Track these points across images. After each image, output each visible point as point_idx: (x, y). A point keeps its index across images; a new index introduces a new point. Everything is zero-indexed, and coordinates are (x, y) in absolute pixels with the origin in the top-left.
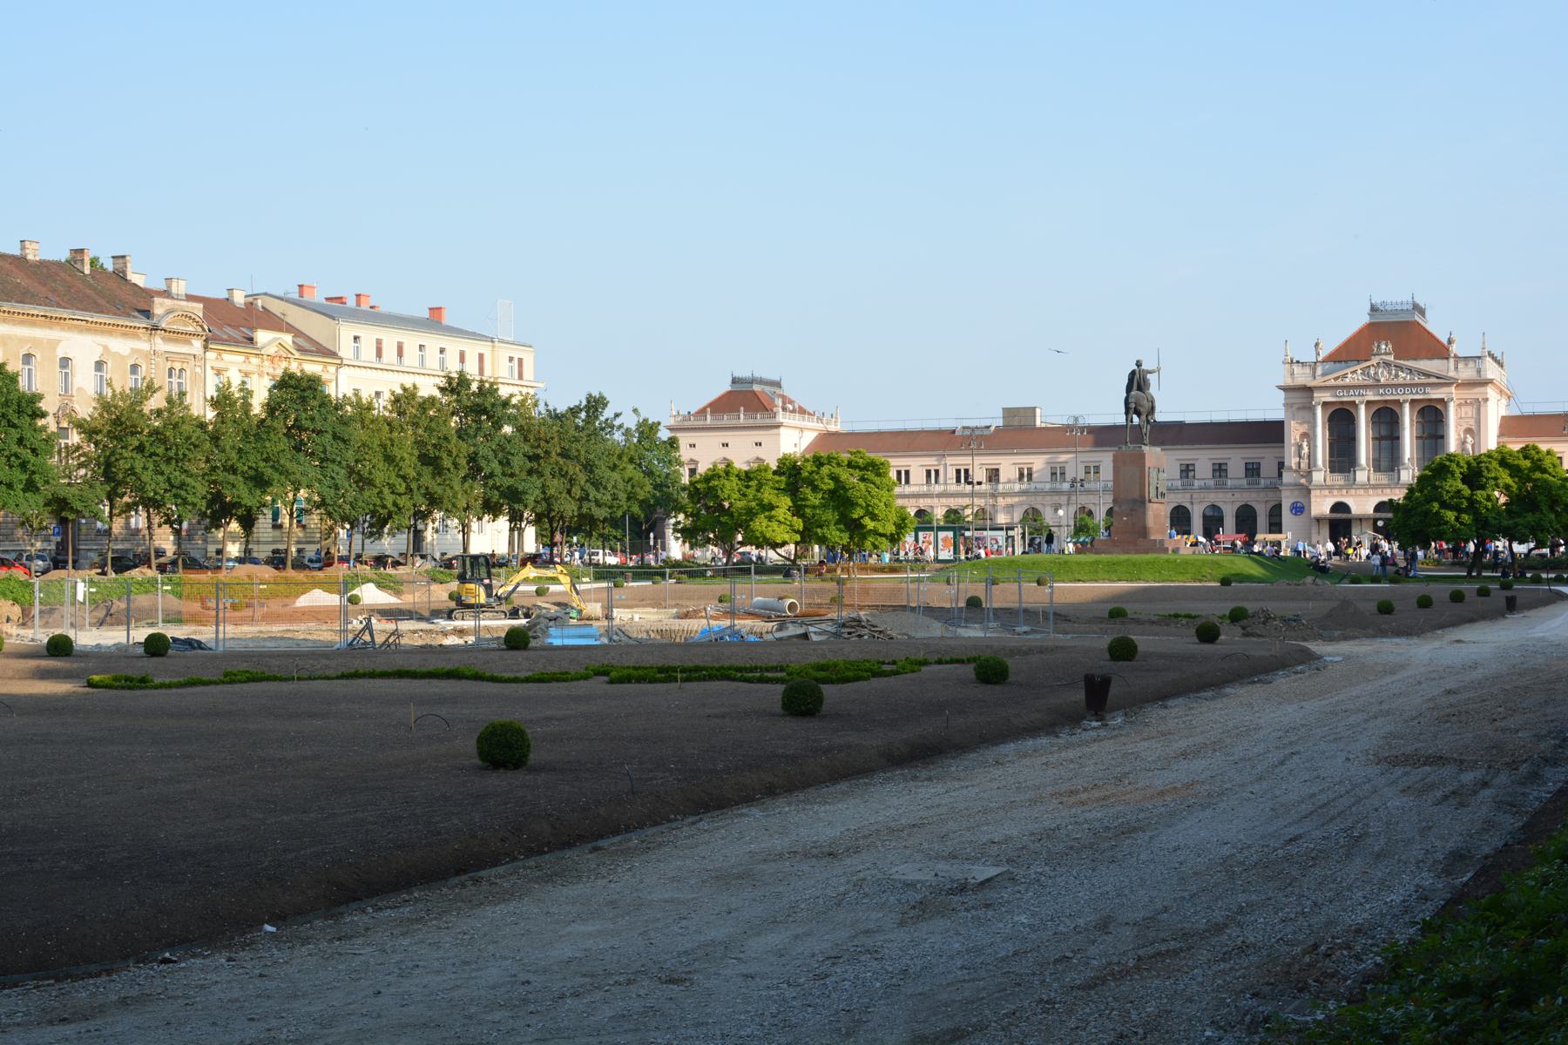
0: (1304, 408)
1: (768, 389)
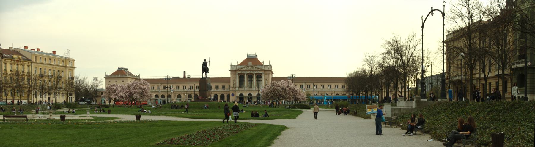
1: (125, 70)
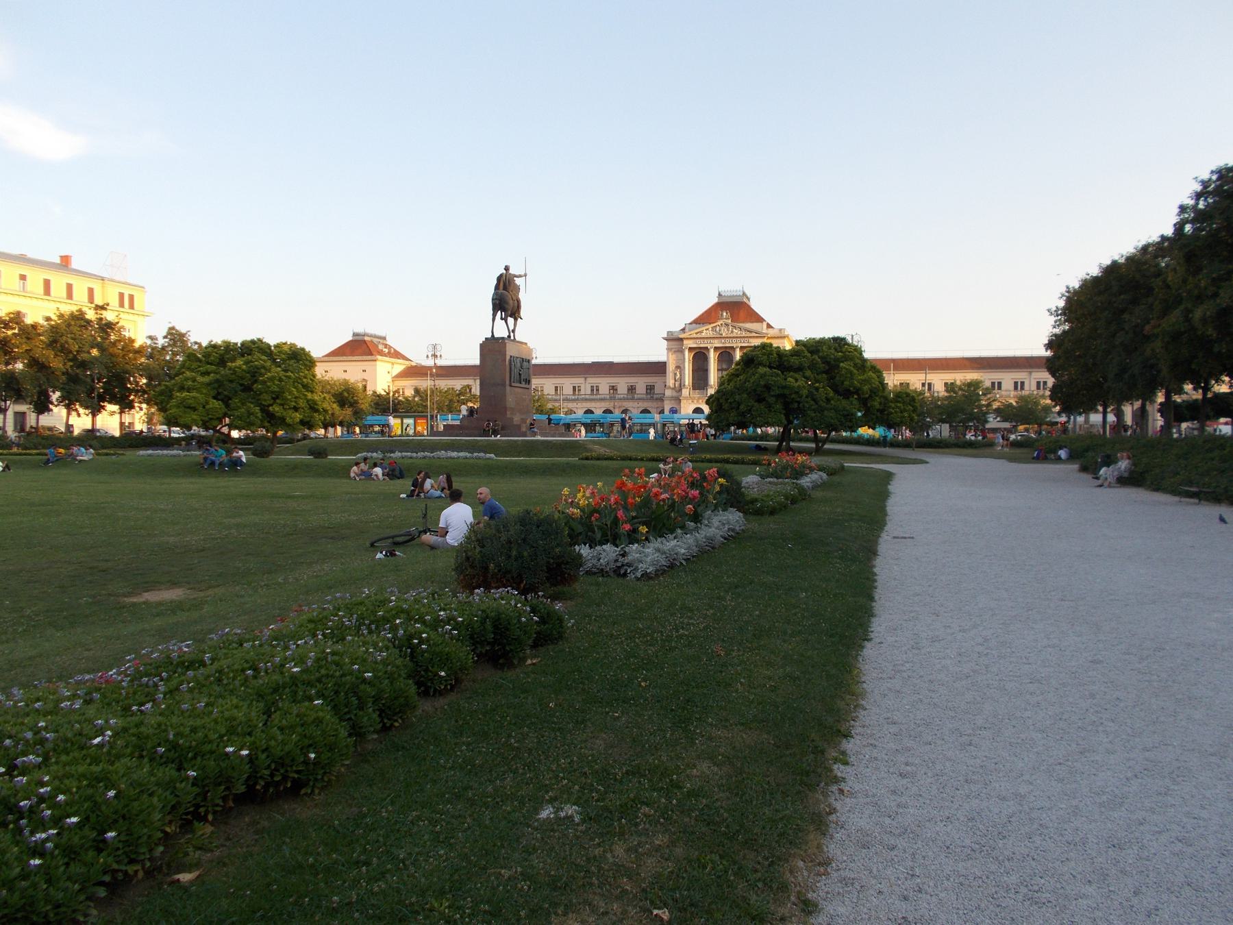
0: (678, 351)
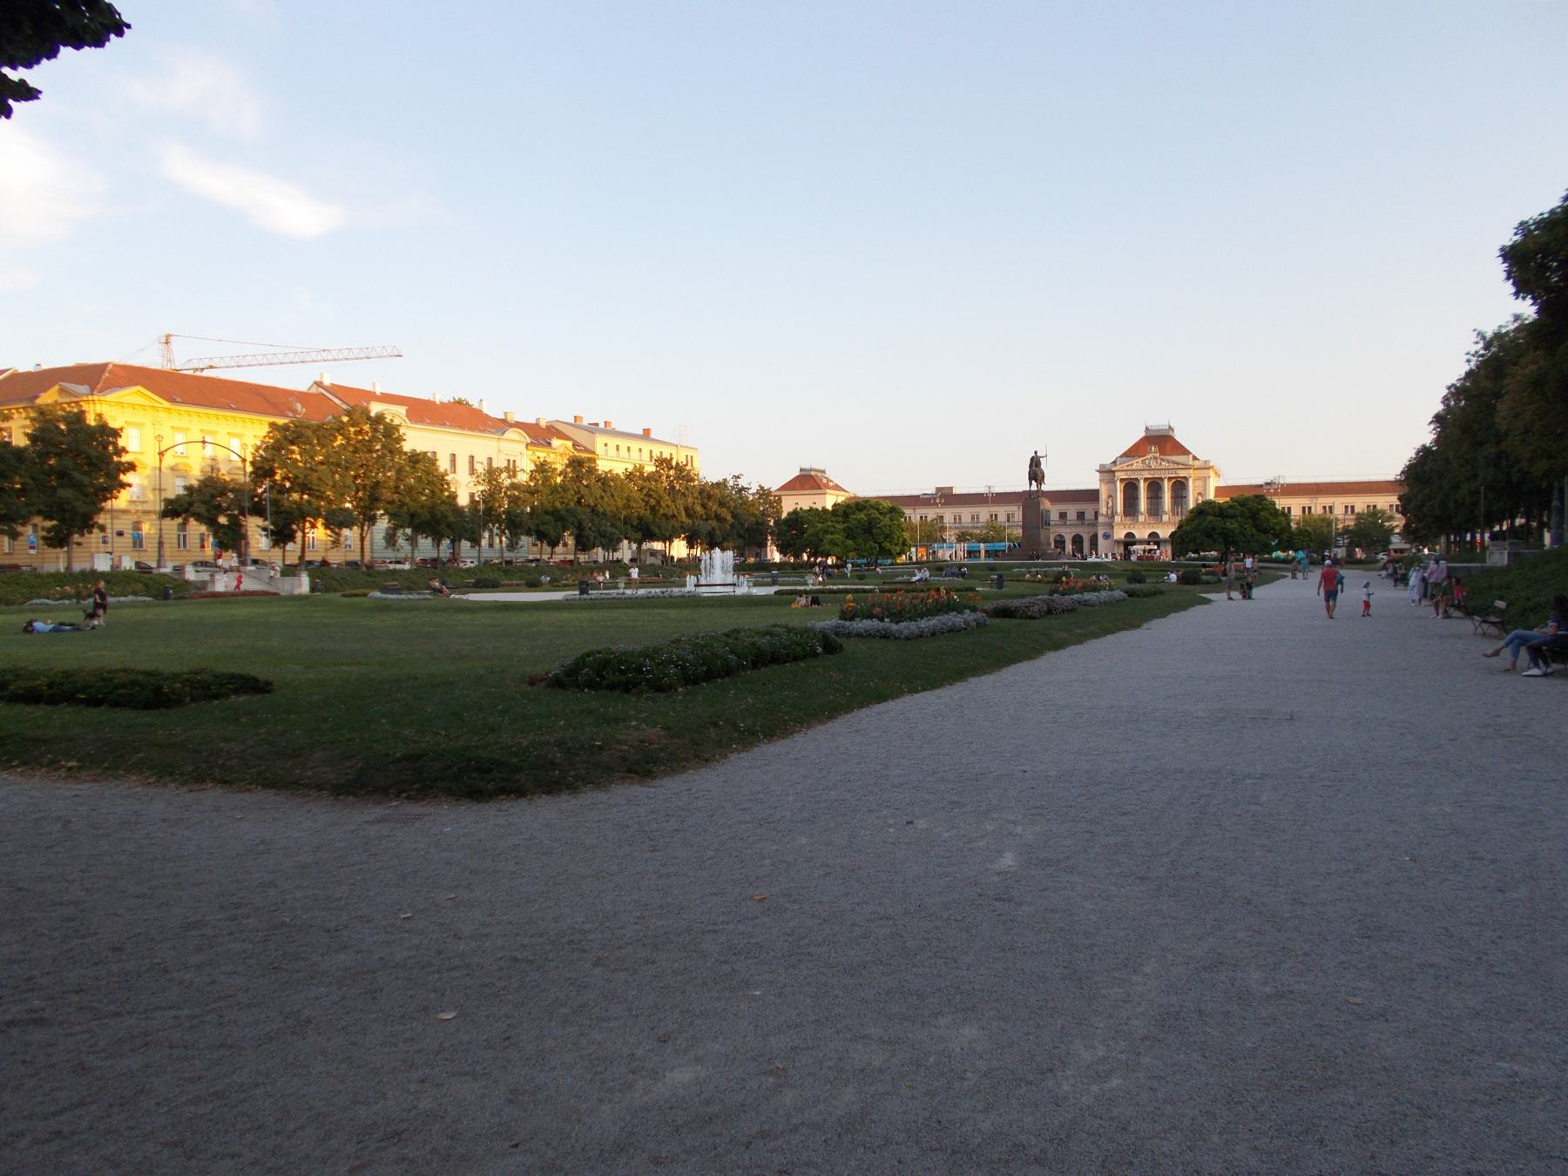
1: (819, 474)
